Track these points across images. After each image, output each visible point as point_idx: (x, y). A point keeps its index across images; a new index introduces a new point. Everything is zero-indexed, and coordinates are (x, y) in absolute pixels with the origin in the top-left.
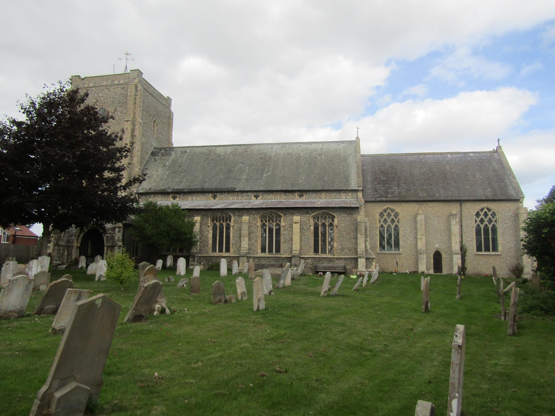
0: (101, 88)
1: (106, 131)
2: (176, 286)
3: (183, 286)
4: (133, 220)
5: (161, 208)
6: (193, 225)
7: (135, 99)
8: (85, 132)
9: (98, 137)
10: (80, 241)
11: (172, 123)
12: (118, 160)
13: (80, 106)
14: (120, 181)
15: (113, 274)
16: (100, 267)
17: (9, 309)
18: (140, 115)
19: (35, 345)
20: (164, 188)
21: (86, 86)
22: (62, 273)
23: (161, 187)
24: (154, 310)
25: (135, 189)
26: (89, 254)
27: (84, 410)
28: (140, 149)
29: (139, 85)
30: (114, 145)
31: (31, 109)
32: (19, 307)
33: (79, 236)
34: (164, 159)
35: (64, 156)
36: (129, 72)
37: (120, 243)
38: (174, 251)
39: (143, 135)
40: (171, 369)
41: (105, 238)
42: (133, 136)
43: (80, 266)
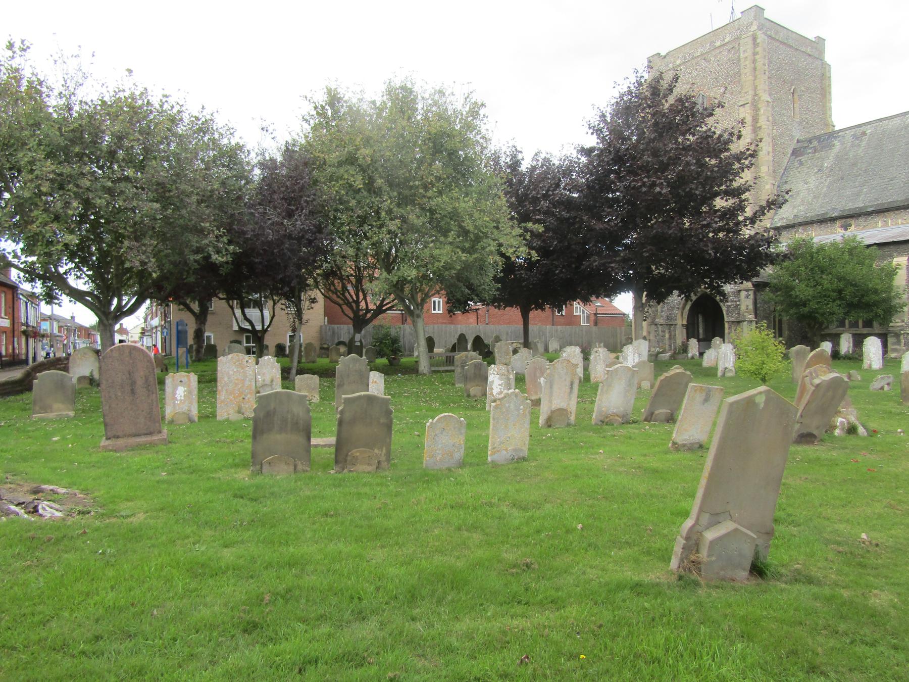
0: (694, 62)
1: (713, 130)
2: (868, 388)
3: (882, 388)
4: (770, 275)
5: (821, 249)
6: (891, 273)
7: (754, 61)
8: (680, 140)
9: (701, 143)
10: (685, 316)
11: (830, 86)
12: (736, 174)
13: (666, 101)
14: (742, 209)
15: (748, 366)
16: (722, 354)
17: (611, 411)
18: (767, 88)
19: (653, 463)
20: (822, 211)
21: (671, 66)
22: (666, 365)
23: (818, 210)
24: (835, 427)
25: (767, 222)
26: (701, 337)
27: (748, 567)
28: (770, 149)
29: (759, 33)
30: (728, 150)
31: (602, 125)
32: (622, 409)
33: (684, 308)
34: (818, 159)
35: (654, 185)
36: (740, 16)
37: (752, 317)
38: (854, 325)
39: (774, 123)
40: (893, 532)
41: (724, 309)
42: (756, 129)
43: (690, 355)
